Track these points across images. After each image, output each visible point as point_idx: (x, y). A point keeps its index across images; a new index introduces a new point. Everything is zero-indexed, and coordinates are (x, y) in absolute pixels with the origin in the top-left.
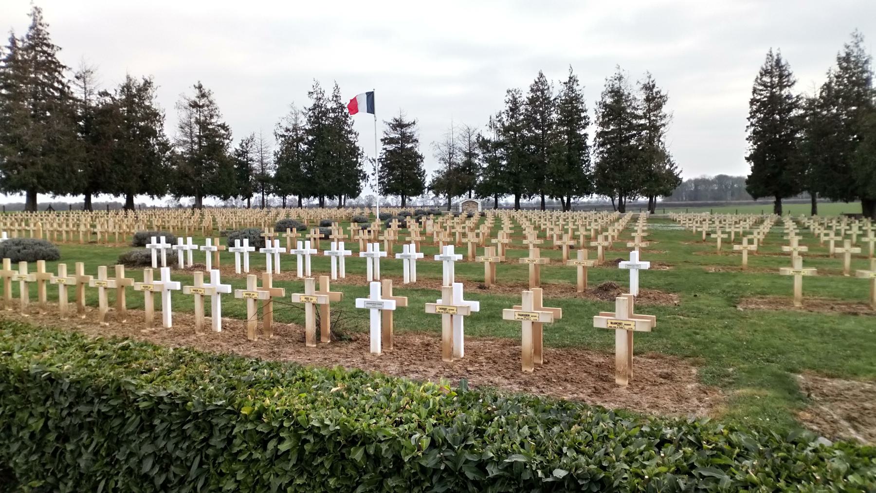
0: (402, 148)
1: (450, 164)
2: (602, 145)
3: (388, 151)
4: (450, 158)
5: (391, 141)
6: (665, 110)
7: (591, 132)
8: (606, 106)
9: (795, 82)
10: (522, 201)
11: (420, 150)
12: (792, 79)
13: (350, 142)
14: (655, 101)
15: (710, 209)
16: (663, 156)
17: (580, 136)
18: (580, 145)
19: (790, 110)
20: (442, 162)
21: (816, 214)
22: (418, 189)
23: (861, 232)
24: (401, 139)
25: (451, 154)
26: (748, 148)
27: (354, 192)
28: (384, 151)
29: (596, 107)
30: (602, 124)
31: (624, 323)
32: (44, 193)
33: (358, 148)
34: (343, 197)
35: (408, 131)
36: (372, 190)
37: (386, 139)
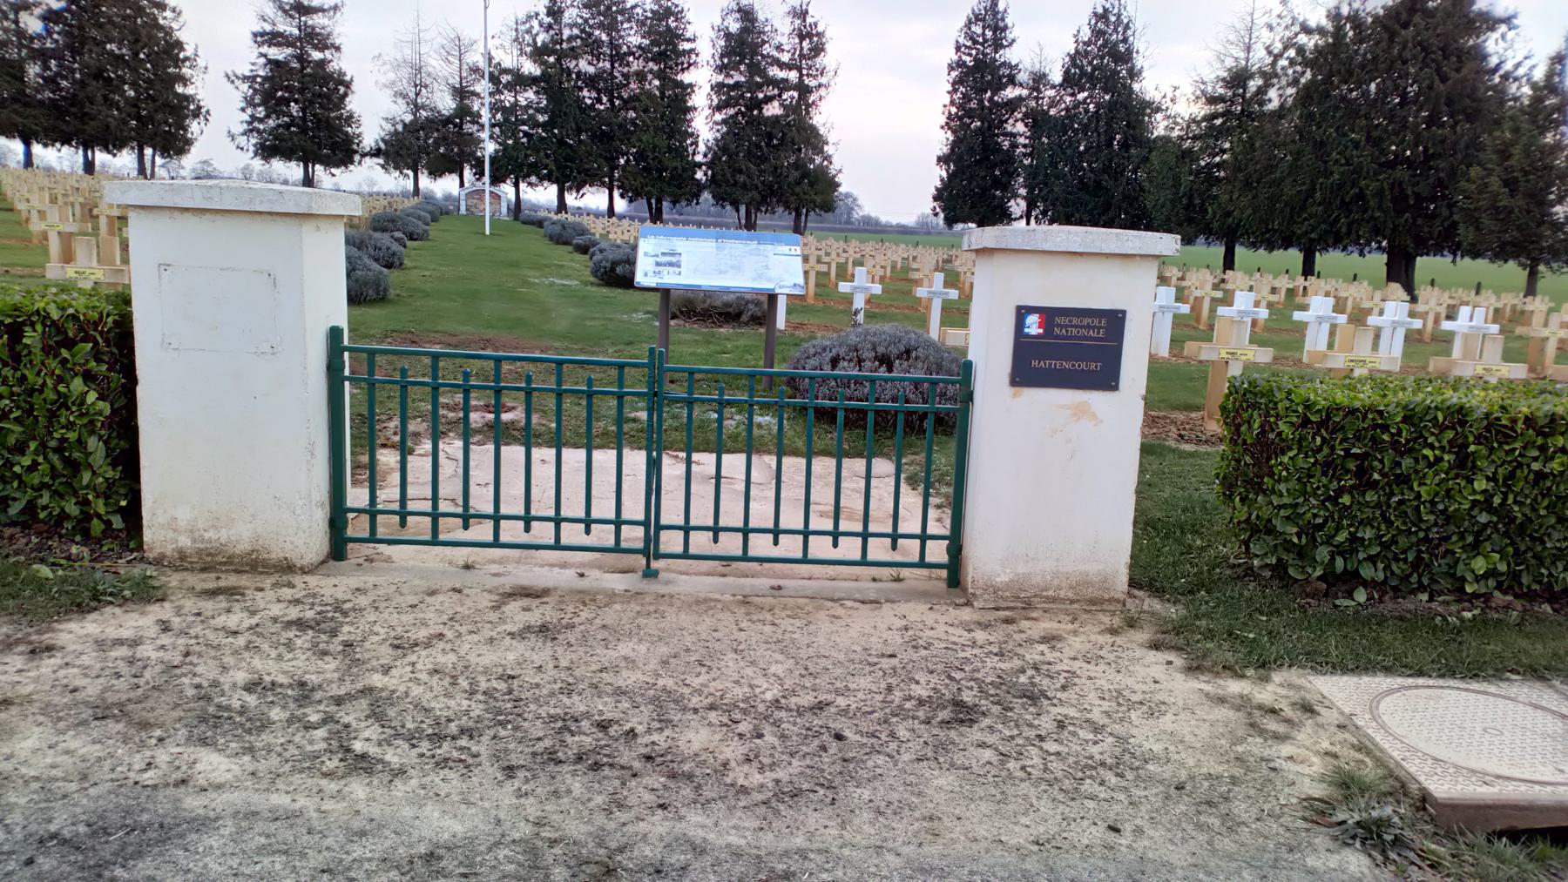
0: (302, 58)
1: (417, 108)
2: (719, 108)
3: (270, 61)
4: (417, 95)
5: (274, 38)
6: (825, 60)
7: (701, 78)
8: (728, 36)
9: (1013, 41)
10: (570, 199)
11: (341, 63)
12: (1010, 36)
13: (161, 28)
14: (811, 41)
15: (843, 235)
16: (814, 140)
17: (681, 85)
18: (677, 102)
19: (1004, 87)
20: (400, 100)
21: (1232, 268)
22: (341, 151)
23: (1219, 294)
24: (299, 39)
25: (419, 86)
26: (941, 141)
27: (174, 144)
28: (262, 60)
29: (713, 35)
30: (721, 69)
31: (1368, 360)
32: (1254, 246)
33: (179, 45)
34: (148, 151)
35: (317, 20)
36: (232, 146)
37: (262, 34)
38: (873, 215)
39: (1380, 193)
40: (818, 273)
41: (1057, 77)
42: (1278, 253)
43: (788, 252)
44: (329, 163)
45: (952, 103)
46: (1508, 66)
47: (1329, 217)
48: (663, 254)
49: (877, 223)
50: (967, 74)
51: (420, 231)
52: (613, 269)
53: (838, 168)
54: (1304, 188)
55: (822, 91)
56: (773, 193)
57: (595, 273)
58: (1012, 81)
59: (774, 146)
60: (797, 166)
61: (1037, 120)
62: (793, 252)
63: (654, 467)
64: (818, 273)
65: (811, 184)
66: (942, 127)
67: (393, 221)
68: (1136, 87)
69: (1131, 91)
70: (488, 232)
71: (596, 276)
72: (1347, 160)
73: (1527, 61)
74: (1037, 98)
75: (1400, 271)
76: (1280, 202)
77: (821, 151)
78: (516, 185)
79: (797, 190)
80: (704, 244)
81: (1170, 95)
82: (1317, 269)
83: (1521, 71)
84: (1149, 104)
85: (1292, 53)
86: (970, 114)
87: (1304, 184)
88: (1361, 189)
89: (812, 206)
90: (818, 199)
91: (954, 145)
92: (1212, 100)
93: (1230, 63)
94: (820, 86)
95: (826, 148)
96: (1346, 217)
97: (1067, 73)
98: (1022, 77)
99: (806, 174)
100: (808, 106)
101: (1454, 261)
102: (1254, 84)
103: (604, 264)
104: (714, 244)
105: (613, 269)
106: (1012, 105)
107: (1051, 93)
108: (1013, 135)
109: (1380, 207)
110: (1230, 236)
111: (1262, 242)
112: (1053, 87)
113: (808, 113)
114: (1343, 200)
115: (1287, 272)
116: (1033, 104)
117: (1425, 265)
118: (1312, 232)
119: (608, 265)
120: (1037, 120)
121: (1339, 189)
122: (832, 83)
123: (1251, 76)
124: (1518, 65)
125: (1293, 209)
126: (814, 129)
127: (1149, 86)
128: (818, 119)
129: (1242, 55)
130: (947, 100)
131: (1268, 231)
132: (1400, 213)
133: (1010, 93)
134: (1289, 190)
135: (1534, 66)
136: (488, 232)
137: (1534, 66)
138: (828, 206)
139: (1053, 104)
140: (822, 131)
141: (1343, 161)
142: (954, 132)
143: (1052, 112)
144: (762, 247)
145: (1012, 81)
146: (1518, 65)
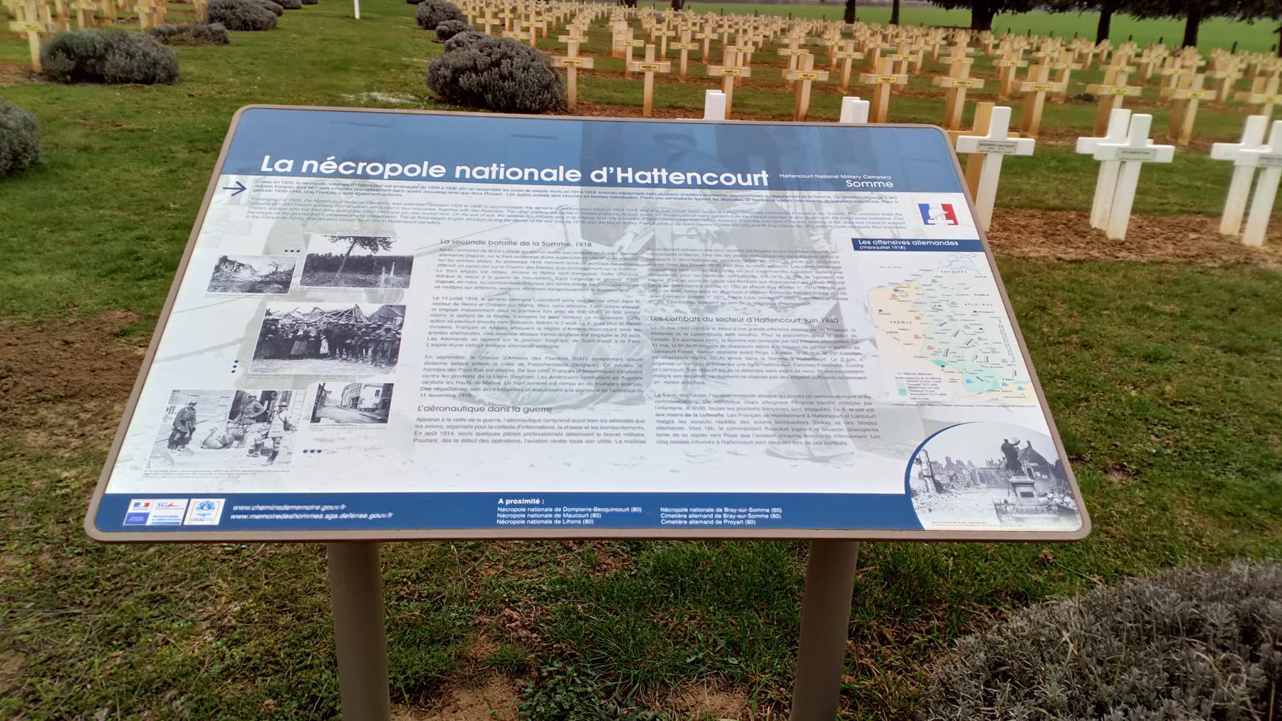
40: (657, 76)
42: (1149, 22)
43: (913, 228)
44: (973, 67)
48: (321, 268)
51: (264, 19)
52: (455, 80)
57: (433, 83)
62: (941, 230)
64: (657, 76)
67: (233, 7)
70: (357, 16)
71: (434, 89)
78: (1184, 146)
80: (530, 198)
82: (993, 26)
103: (443, 71)
104: (571, 198)
105: (455, 80)
119: (448, 73)
136: (357, 16)
144: (793, 203)
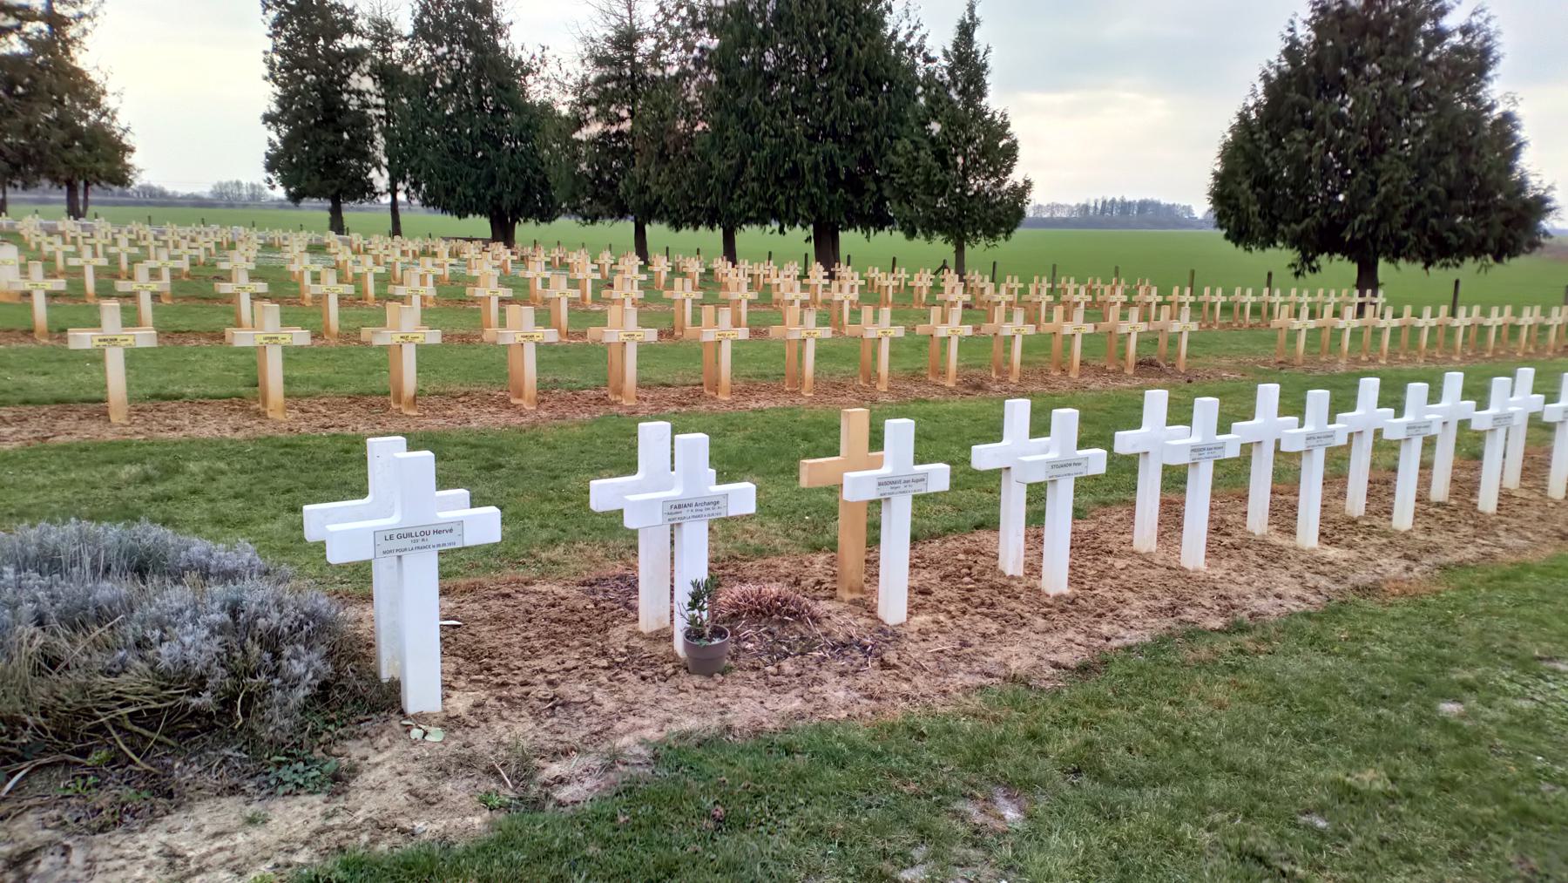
16: (82, 88)
26: (266, 96)
38: (155, 184)
39: (815, 168)
41: (406, 26)
42: (920, 241)
45: (276, 50)
46: (901, 37)
47: (765, 193)
49: (163, 194)
50: (289, 16)
53: (124, 126)
54: (733, 162)
55: (86, 23)
56: (27, 159)
58: (349, 28)
59: (19, 96)
60: (62, 123)
61: (387, 75)
63: (1034, 569)
65: (87, 148)
66: (266, 78)
68: (502, 43)
69: (496, 48)
72: (776, 131)
73: (917, 31)
74: (383, 51)
75: (503, 233)
76: (711, 177)
77: (95, 104)
79: (68, 155)
81: (538, 55)
83: (914, 42)
84: (519, 63)
85: (684, 12)
86: (300, 64)
87: (732, 157)
88: (795, 163)
89: (93, 178)
90: (102, 167)
91: (284, 102)
92: (600, 61)
93: (614, 21)
94: (81, 16)
95: (103, 100)
96: (782, 193)
97: (419, 22)
98: (362, 23)
99: (77, 134)
100: (67, 42)
101: (868, 237)
102: (647, 45)
106: (355, 56)
107: (405, 45)
108: (359, 93)
109: (816, 184)
110: (645, 214)
111: (686, 221)
112: (401, 38)
113: (67, 52)
114: (777, 176)
115: (583, 246)
116: (379, 56)
117: (850, 240)
118: (749, 210)
120: (387, 75)
121: (772, 163)
122: (99, 12)
123: (640, 37)
124: (909, 36)
125: (725, 184)
126: (79, 72)
127: (518, 41)
128: (84, 59)
129: (625, 13)
130: (268, 44)
131: (691, 208)
132: (833, 190)
133: (348, 42)
134: (720, 166)
135: (924, 37)
137: (924, 37)
138: (119, 177)
139: (407, 57)
140: (94, 76)
141: (772, 133)
142: (283, 86)
143: (407, 68)
145: (349, 28)
146: (909, 36)
